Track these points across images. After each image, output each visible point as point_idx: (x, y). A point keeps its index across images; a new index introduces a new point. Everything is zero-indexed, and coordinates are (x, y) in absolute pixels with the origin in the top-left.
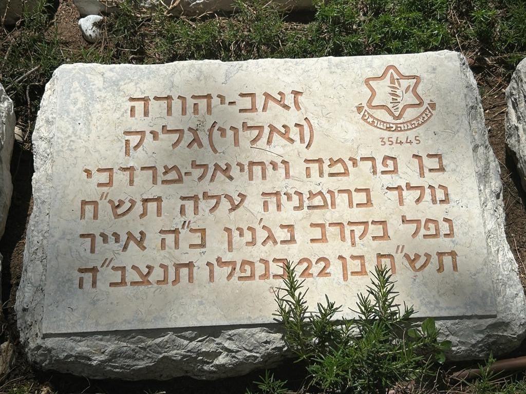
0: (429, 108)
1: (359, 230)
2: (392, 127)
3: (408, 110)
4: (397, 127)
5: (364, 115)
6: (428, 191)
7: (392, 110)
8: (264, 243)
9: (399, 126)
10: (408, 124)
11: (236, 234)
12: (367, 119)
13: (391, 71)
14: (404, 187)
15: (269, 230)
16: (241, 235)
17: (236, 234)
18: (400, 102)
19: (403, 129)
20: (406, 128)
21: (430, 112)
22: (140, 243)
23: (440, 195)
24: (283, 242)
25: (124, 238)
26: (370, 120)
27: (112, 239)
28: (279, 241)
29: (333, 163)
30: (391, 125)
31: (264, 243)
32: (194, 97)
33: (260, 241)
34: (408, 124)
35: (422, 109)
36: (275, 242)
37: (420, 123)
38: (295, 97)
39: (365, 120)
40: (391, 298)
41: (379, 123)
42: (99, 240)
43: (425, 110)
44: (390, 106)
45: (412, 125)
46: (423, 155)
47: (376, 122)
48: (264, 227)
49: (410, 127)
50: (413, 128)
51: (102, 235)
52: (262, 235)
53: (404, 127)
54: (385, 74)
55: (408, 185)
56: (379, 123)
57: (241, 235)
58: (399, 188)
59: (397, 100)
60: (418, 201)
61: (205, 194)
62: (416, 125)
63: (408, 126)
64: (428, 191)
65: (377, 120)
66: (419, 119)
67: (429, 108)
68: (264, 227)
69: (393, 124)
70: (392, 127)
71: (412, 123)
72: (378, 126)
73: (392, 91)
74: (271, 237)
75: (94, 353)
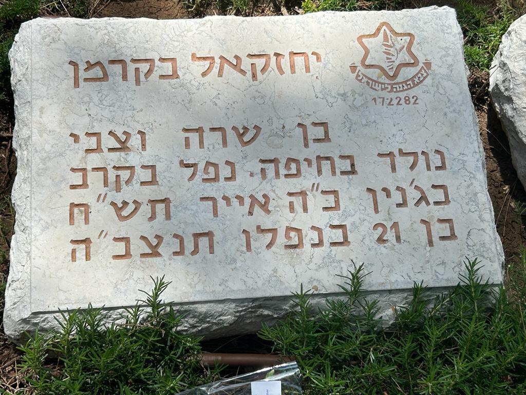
0: (425, 68)
1: (125, 174)
2: (387, 88)
3: (403, 69)
4: (392, 88)
5: (358, 76)
6: (422, 159)
7: (387, 69)
8: (417, 204)
9: (394, 86)
10: (404, 85)
11: (381, 196)
12: (361, 79)
13: (384, 27)
14: (396, 153)
15: (422, 192)
16: (388, 195)
17: (381, 196)
18: (394, 62)
19: (398, 90)
20: (401, 89)
21: (425, 71)
22: (264, 207)
23: (436, 160)
24: (436, 203)
25: (247, 201)
26: (365, 80)
27: (235, 202)
28: (431, 201)
29: (90, 66)
30: (386, 86)
31: (417, 204)
32: (250, 56)
33: (411, 202)
34: (404, 85)
35: (418, 68)
36: (428, 203)
37: (416, 83)
38: (276, 59)
39: (360, 81)
40: (128, 310)
41: (374, 83)
42: (221, 203)
43: (421, 70)
44: (384, 66)
45: (407, 85)
46: (307, 123)
47: (371, 82)
48: (416, 187)
49: (406, 87)
50: (408, 89)
51: (225, 198)
52: (415, 195)
53: (400, 87)
54: (378, 30)
55: (400, 151)
56: (377, 84)
57: (388, 195)
58: (390, 154)
59: (391, 59)
60: (412, 167)
61: (400, 151)
62: (412, 86)
63: (403, 86)
64: (422, 159)
65: (372, 80)
66: (415, 79)
67: (425, 68)
68: (416, 187)
69: (388, 84)
70: (387, 88)
71: (408, 83)
72: (373, 87)
73: (386, 49)
74: (423, 198)
75: (426, 301)
